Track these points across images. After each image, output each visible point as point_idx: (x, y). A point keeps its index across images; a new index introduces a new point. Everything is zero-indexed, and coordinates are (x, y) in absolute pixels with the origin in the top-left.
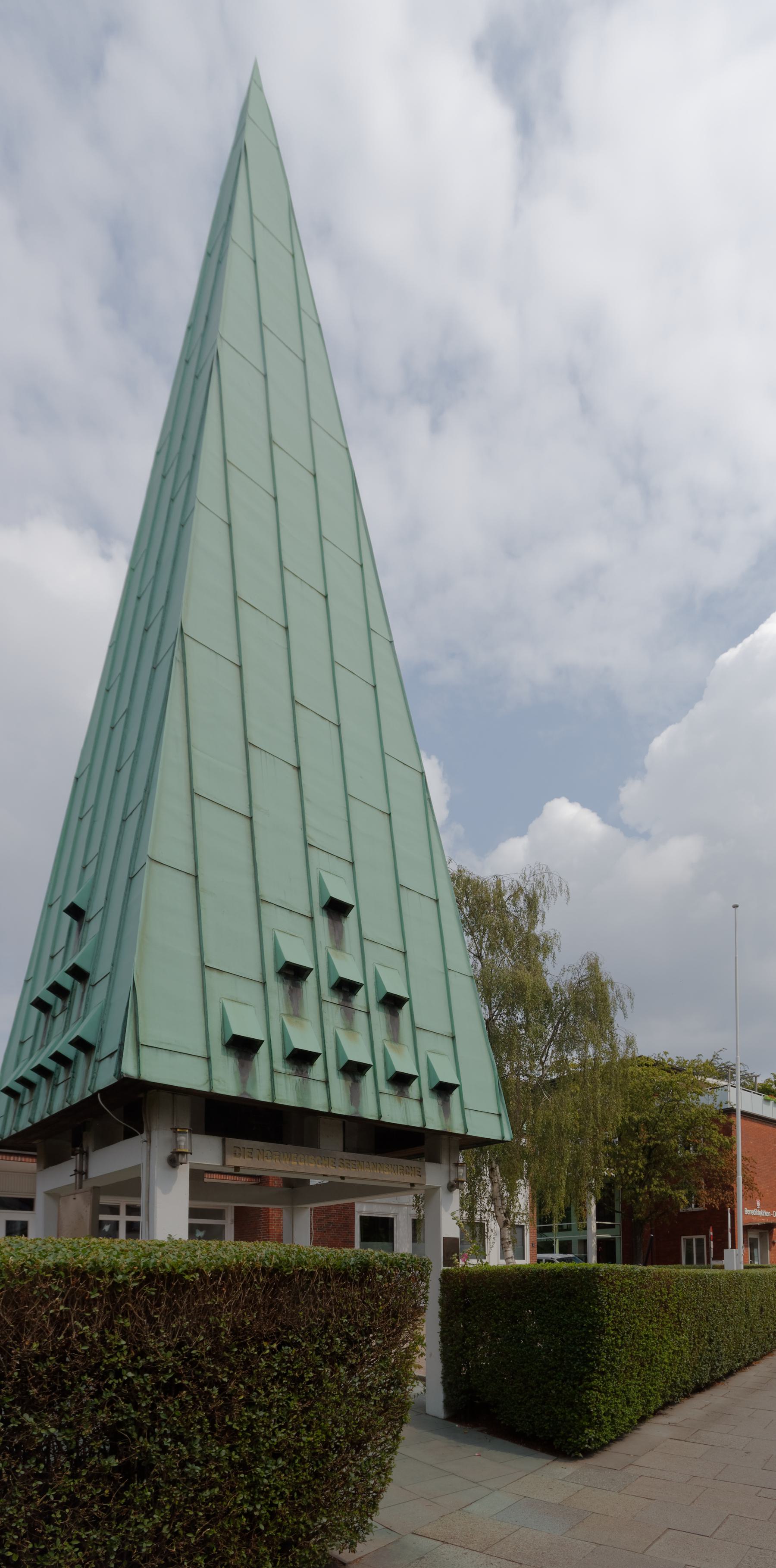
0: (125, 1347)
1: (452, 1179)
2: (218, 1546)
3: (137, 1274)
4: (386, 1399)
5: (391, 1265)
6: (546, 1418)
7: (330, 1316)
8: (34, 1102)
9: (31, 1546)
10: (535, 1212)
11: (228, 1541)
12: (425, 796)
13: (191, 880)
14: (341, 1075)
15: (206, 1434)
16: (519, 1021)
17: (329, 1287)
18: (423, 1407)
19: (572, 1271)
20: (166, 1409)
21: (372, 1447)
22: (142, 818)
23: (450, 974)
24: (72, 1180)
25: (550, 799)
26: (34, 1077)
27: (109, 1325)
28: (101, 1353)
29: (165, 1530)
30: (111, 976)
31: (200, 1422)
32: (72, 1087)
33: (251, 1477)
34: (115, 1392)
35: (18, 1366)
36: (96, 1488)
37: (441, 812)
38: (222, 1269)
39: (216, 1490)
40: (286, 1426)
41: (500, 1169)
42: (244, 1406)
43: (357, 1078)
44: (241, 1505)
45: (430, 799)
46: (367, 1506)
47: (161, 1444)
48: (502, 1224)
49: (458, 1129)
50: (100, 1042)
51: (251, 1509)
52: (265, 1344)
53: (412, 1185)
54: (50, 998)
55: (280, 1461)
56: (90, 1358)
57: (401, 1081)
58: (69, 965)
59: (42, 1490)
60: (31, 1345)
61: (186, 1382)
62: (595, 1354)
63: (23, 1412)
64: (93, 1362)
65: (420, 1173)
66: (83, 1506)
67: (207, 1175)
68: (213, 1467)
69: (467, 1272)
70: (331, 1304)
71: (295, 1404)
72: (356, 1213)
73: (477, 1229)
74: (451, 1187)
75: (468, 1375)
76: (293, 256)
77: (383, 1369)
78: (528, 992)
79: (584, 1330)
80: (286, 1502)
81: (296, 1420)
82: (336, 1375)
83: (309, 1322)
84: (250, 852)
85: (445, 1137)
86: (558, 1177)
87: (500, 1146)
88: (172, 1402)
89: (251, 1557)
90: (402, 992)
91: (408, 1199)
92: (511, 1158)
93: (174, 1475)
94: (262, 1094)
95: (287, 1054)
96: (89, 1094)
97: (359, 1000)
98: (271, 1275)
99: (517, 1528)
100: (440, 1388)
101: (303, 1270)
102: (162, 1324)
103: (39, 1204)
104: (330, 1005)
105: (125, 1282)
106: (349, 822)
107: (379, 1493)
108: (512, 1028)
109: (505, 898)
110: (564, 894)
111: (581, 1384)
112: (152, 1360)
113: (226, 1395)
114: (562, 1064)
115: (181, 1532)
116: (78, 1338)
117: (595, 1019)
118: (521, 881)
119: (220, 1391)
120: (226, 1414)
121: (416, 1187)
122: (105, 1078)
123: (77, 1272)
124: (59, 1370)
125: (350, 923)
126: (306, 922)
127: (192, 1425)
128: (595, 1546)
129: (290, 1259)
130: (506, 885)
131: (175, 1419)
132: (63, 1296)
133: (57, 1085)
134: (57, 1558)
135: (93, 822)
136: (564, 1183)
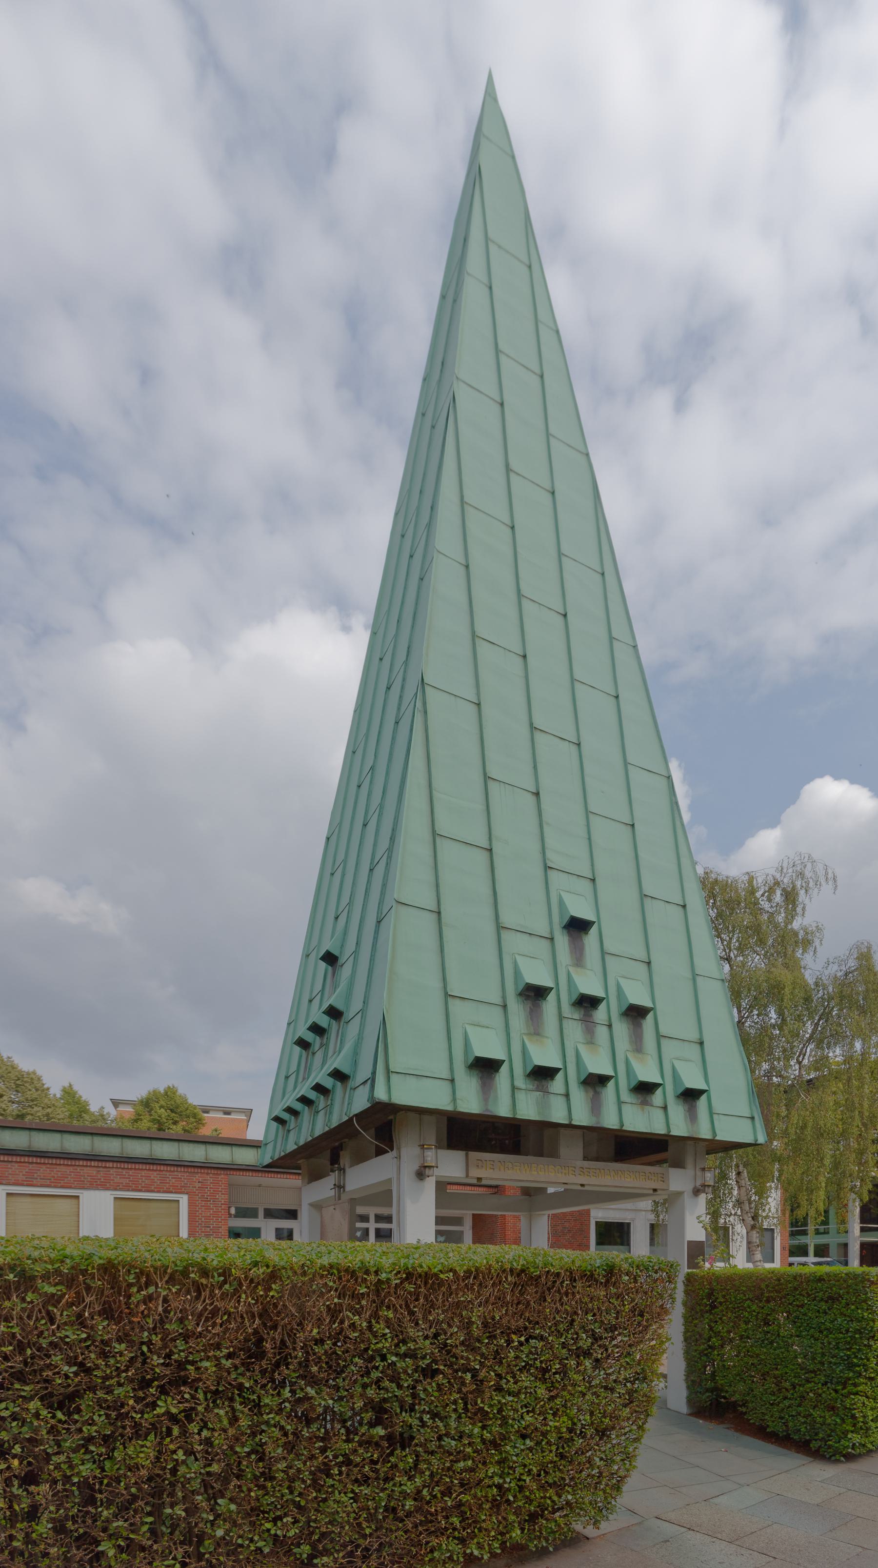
0: (389, 1335)
1: (698, 1183)
2: (471, 1510)
3: (399, 1272)
4: (630, 1393)
5: (638, 1267)
7: (576, 1313)
8: (299, 1127)
9: (314, 1494)
10: (787, 1215)
11: (480, 1507)
12: (671, 800)
13: (435, 916)
15: (460, 1414)
16: (773, 1021)
17: (575, 1287)
18: (665, 1402)
19: (836, 1275)
21: (617, 1436)
22: (388, 864)
23: (699, 979)
25: (810, 779)
26: (298, 1106)
27: (376, 1315)
28: (369, 1339)
29: (425, 1492)
30: (363, 1012)
31: (455, 1402)
32: (331, 1113)
33: (501, 1453)
34: (382, 1372)
35: (302, 1348)
36: (367, 1452)
37: (686, 817)
38: (473, 1270)
39: (470, 1463)
40: (533, 1411)
41: (748, 1173)
42: (495, 1390)
43: (598, 1089)
44: (492, 1477)
45: (677, 803)
46: (611, 1489)
47: (421, 1419)
48: (749, 1228)
49: (705, 1133)
50: (355, 1072)
51: (501, 1481)
52: (514, 1337)
53: (655, 1190)
54: (309, 1037)
55: (528, 1442)
56: (360, 1343)
57: (644, 1089)
58: (325, 1006)
59: (323, 1450)
60: (312, 1331)
61: (442, 1367)
62: (862, 1359)
63: (306, 1385)
64: (363, 1346)
65: (664, 1178)
66: (356, 1465)
67: (449, 1187)
68: (467, 1442)
69: (714, 1274)
70: (576, 1302)
71: (542, 1392)
72: (592, 1219)
73: (721, 1232)
74: (696, 1192)
75: (713, 1374)
76: (530, 267)
77: (628, 1363)
78: (786, 990)
79: (850, 1334)
80: (533, 1478)
81: (542, 1407)
82: (582, 1368)
83: (554, 1318)
84: (491, 882)
85: (689, 1142)
86: (817, 1179)
87: (750, 1149)
88: (430, 1384)
89: (501, 1523)
90: (646, 1003)
91: (646, 1204)
92: (762, 1161)
93: (432, 1446)
94: (503, 1110)
95: (528, 1072)
96: (345, 1118)
98: (518, 1275)
99: (770, 1523)
100: (683, 1385)
101: (548, 1272)
102: (421, 1316)
103: (305, 1213)
104: (570, 1021)
105: (388, 1279)
106: (589, 839)
107: (623, 1478)
108: (764, 1029)
109: (758, 894)
110: (830, 883)
112: (412, 1347)
113: (477, 1380)
114: (820, 1063)
115: (439, 1495)
116: (350, 1326)
117: (865, 1012)
118: (778, 876)
119: (473, 1377)
120: (478, 1397)
121: (659, 1192)
122: (360, 1103)
123: (347, 1270)
124: (335, 1353)
125: (591, 939)
126: (545, 944)
127: (447, 1405)
128: (860, 1550)
129: (537, 1262)
130: (760, 880)
131: (433, 1398)
132: (336, 1290)
133: (318, 1112)
134: (336, 1506)
135: (343, 875)
136: (823, 1185)
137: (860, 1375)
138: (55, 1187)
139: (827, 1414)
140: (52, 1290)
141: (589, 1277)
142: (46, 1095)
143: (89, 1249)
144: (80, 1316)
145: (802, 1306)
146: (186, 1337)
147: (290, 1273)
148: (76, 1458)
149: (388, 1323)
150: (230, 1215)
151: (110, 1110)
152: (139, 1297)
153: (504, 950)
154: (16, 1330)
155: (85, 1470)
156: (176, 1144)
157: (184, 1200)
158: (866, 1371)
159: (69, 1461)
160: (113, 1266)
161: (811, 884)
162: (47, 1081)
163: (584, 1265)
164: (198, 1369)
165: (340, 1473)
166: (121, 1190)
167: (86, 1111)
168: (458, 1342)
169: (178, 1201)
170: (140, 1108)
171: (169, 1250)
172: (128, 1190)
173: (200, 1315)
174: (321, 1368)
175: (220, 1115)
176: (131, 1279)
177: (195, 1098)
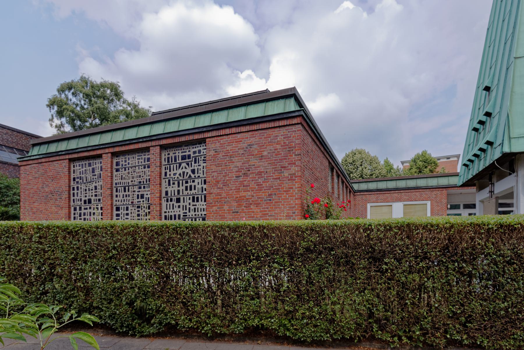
8: (473, 167)
20: (508, 270)
24: (488, 195)
26: (473, 158)
54: (478, 126)
93: (512, 292)
96: (492, 162)
122: (497, 155)
123: (477, 225)
135: (494, 46)
140: (396, 231)
144: (402, 238)
148: (401, 275)
149: (493, 244)
151: (401, 166)
152: (415, 233)
156: (425, 179)
157: (429, 203)
159: (400, 276)
164: (430, 254)
166: (406, 201)
167: (392, 168)
169: (426, 204)
170: (412, 163)
173: (431, 238)
175: (445, 160)
176: (414, 228)
177: (434, 154)
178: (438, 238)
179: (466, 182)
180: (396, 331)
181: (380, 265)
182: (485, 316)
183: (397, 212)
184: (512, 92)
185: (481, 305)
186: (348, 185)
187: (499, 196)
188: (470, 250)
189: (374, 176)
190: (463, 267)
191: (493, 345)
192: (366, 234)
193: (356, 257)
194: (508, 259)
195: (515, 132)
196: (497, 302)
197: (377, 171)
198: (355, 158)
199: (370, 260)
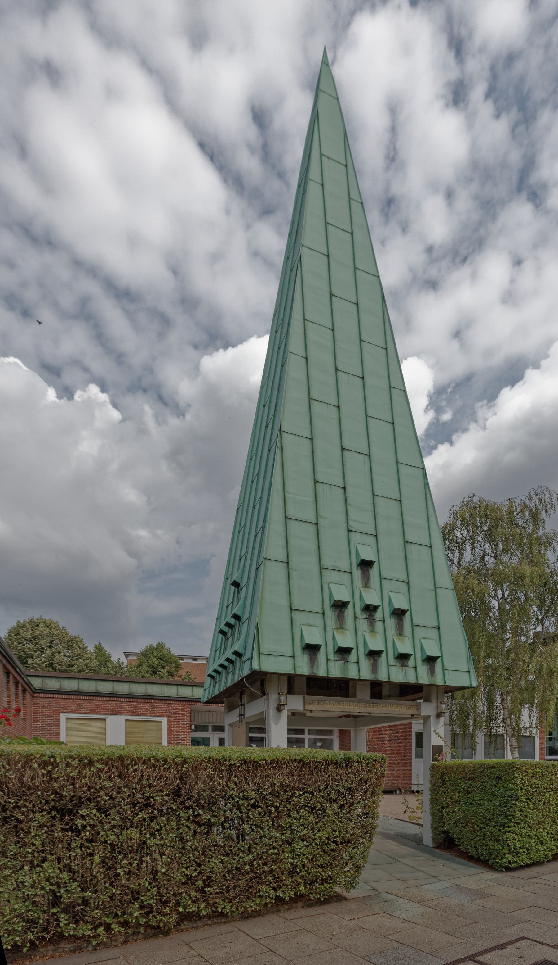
6: (485, 848)
8: (220, 681)
14: (367, 658)
20: (253, 815)
24: (238, 719)
27: (229, 780)
30: (249, 619)
31: (267, 821)
39: (276, 851)
40: (307, 827)
45: (428, 484)
49: (439, 681)
51: (292, 861)
52: (296, 791)
53: (413, 715)
54: (226, 629)
57: (403, 658)
61: (260, 804)
63: (199, 809)
64: (223, 793)
65: (418, 708)
71: (311, 819)
72: (413, 730)
74: (438, 716)
76: (346, 166)
84: (317, 542)
86: (549, 703)
93: (257, 841)
96: (240, 678)
97: (378, 615)
98: (299, 763)
100: (430, 830)
104: (361, 620)
111: (504, 829)
118: (527, 502)
126: (347, 576)
135: (244, 534)
137: (511, 821)
138: (93, 714)
139: (496, 844)
140: (100, 766)
141: (336, 764)
142: (86, 652)
143: (113, 750)
144: (110, 777)
145: (485, 782)
146: (150, 786)
147: (192, 760)
150: (192, 730)
152: (132, 770)
153: (323, 581)
154: (88, 782)
155: (113, 838)
156: (160, 686)
157: (165, 720)
158: (514, 819)
160: (122, 757)
161: (549, 506)
162: (86, 643)
163: (333, 758)
164: (154, 800)
165: (215, 850)
166: (129, 715)
167: (110, 661)
168: (268, 793)
171: (144, 751)
172: (133, 715)
174: (205, 802)
175: (191, 661)
176: (129, 762)
178: (166, 777)
179: (212, 698)
180: (100, 919)
181: (71, 820)
182: (227, 875)
183: (115, 732)
184: (262, 598)
185: (222, 862)
186: (19, 678)
187: (250, 721)
188: (208, 792)
189: (75, 668)
190: (199, 815)
191: (237, 909)
192: (44, 771)
193: (24, 810)
194: (253, 801)
195: (266, 647)
196: (241, 855)
197: (80, 660)
198: (37, 632)
199: (54, 813)
